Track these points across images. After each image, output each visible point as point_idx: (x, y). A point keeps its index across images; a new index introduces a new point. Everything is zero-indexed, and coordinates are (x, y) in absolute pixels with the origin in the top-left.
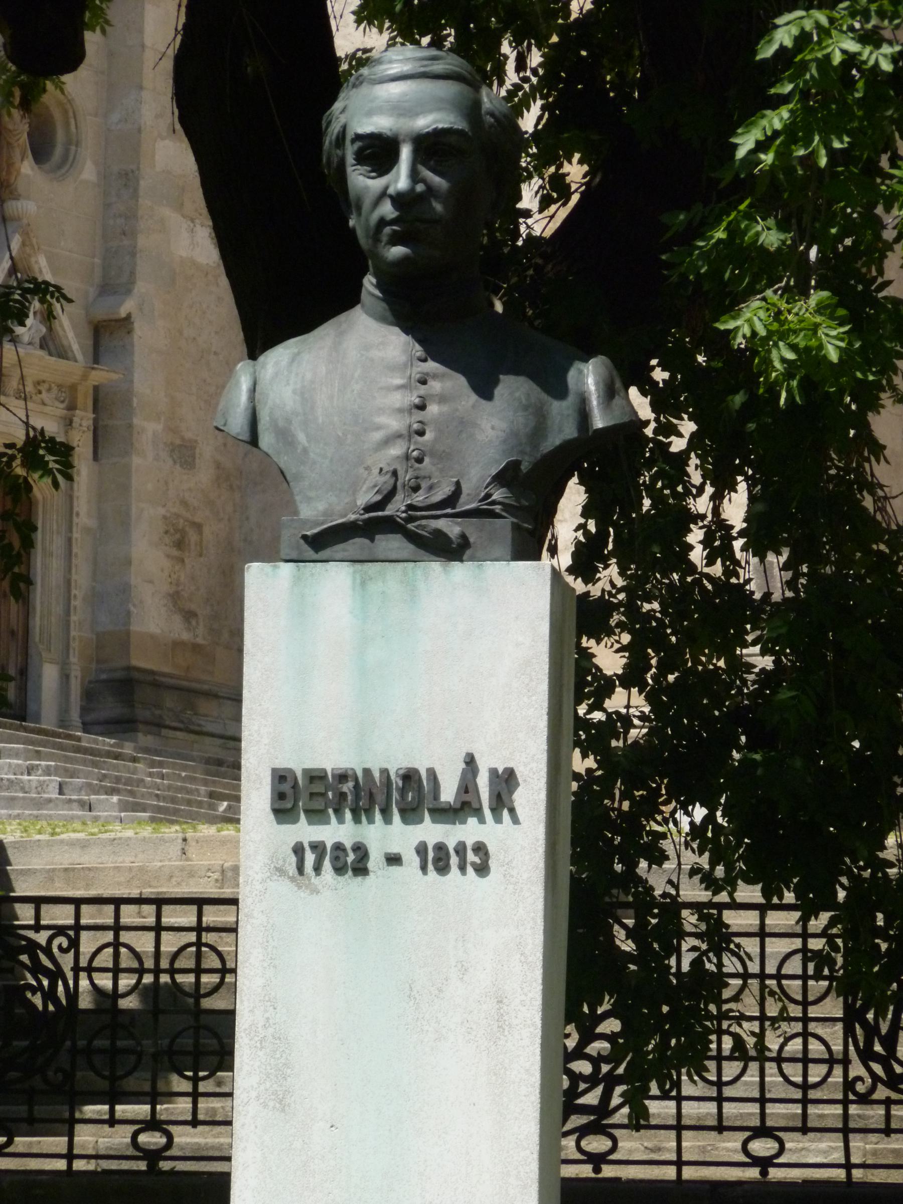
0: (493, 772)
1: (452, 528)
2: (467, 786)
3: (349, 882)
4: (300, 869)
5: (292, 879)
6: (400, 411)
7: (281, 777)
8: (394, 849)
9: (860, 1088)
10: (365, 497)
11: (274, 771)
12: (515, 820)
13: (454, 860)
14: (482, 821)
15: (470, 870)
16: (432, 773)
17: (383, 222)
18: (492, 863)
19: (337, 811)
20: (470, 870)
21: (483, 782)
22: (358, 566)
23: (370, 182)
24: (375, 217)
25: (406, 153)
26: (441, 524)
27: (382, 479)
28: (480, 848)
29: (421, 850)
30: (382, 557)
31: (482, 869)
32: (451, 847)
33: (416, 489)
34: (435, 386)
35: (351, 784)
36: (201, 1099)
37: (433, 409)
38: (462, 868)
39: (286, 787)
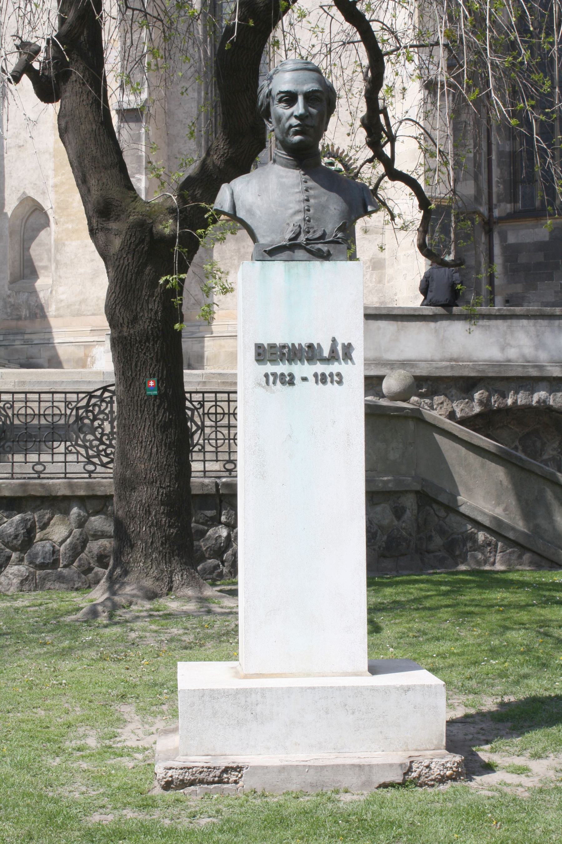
0: (343, 345)
1: (325, 248)
2: (333, 350)
3: (287, 388)
4: (267, 383)
5: (263, 387)
6: (299, 201)
7: (259, 347)
8: (304, 375)
9: (200, 448)
10: (288, 235)
11: (256, 344)
12: (353, 363)
13: (329, 379)
14: (340, 364)
15: (335, 383)
16: (319, 345)
17: (291, 126)
18: (344, 380)
19: (281, 360)
20: (335, 383)
21: (339, 348)
22: (287, 263)
23: (285, 111)
24: (287, 125)
25: (300, 99)
26: (320, 246)
27: (295, 228)
28: (339, 375)
29: (316, 375)
30: (296, 259)
31: (340, 382)
32: (327, 374)
33: (308, 232)
34: (312, 192)
35: (287, 350)
36: (55, 455)
37: (312, 201)
38: (332, 382)
39: (261, 351)
